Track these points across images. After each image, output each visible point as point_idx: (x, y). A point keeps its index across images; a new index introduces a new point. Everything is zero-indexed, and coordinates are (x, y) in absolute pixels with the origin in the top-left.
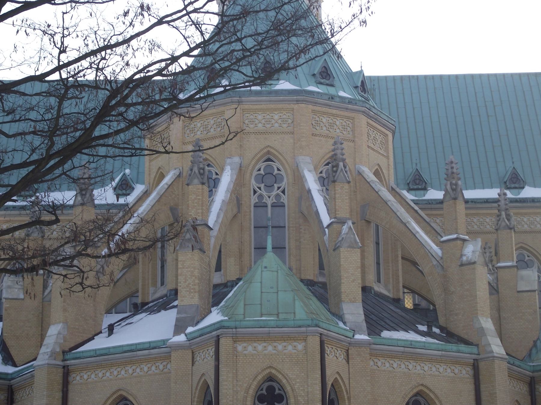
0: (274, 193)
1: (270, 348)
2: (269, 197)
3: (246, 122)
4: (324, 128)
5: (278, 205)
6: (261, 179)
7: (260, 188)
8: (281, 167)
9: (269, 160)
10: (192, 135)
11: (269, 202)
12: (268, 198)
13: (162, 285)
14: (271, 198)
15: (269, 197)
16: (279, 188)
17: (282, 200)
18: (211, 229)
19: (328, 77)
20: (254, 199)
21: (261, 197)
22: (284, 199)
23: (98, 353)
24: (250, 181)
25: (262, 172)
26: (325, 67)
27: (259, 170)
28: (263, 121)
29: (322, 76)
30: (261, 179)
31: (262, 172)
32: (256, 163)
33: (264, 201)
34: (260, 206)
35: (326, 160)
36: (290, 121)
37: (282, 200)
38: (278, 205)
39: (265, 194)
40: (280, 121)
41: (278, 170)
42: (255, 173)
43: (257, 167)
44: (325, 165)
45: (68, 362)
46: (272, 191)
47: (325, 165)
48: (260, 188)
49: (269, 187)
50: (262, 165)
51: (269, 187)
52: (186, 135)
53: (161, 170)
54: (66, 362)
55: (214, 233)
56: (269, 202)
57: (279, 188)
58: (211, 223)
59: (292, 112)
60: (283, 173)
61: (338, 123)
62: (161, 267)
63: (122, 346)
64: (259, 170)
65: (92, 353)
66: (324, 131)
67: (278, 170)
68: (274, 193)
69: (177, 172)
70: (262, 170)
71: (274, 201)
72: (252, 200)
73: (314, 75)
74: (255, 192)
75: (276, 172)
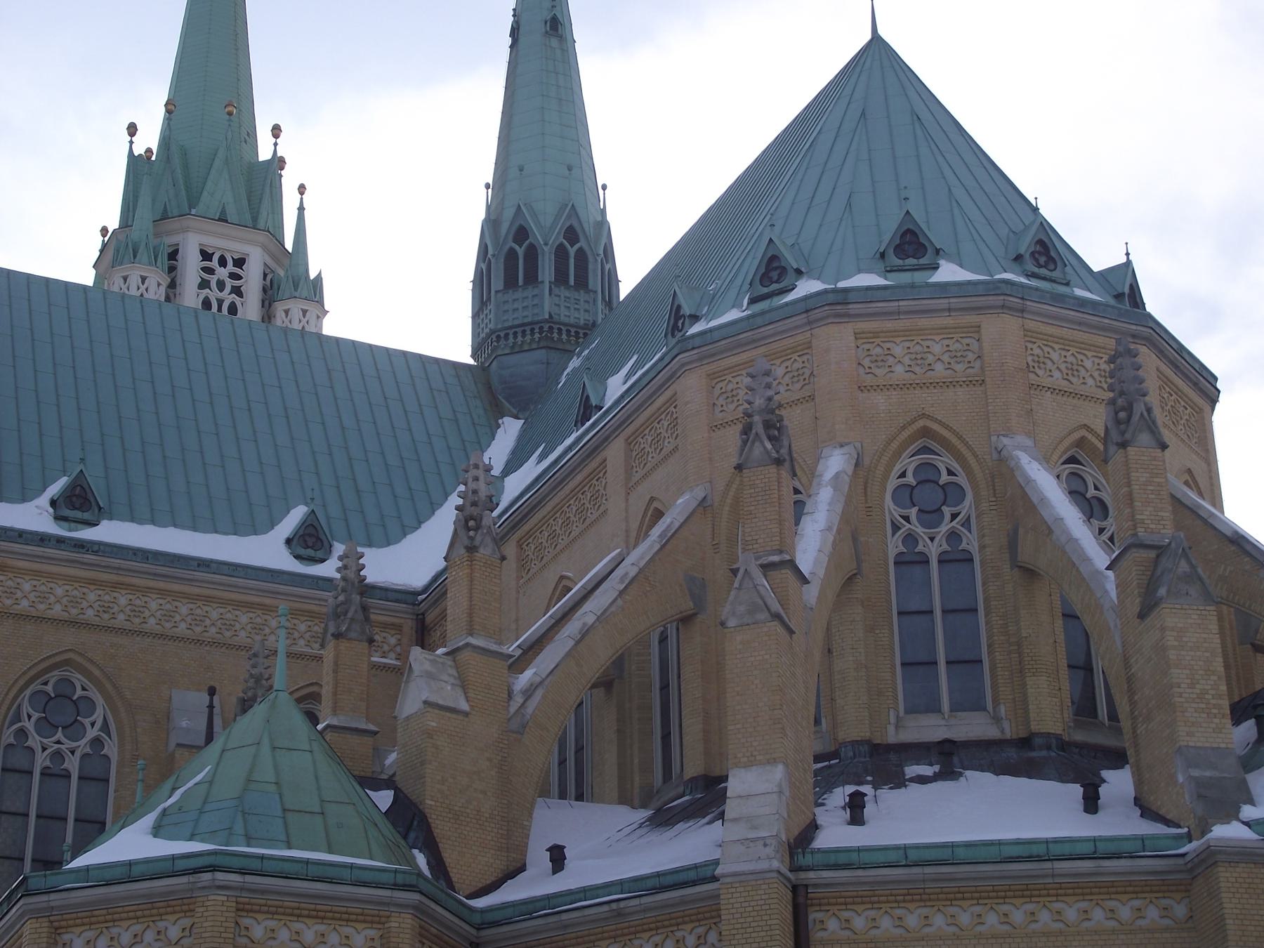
0: (944, 528)
1: (1153, 913)
2: (932, 539)
3: (866, 362)
4: (1057, 374)
5: (956, 559)
6: (906, 494)
7: (907, 519)
8: (956, 466)
9: (925, 450)
10: (732, 407)
11: (934, 551)
12: (929, 541)
13: (664, 782)
14: (936, 540)
15: (932, 539)
16: (954, 516)
17: (964, 545)
18: (805, 580)
19: (1052, 267)
20: (894, 546)
21: (911, 539)
22: (971, 542)
23: (913, 855)
24: (882, 499)
25: (910, 479)
26: (1041, 242)
27: (903, 475)
28: (907, 361)
29: (1037, 260)
30: (906, 494)
31: (910, 479)
32: (897, 455)
33: (920, 548)
34: (911, 561)
35: (1064, 452)
36: (971, 356)
37: (964, 545)
38: (956, 559)
39: (920, 530)
40: (946, 358)
41: (950, 473)
42: (893, 483)
43: (897, 469)
44: (1064, 463)
45: (811, 875)
46: (937, 524)
47: (1064, 463)
48: (907, 519)
49: (931, 516)
50: (909, 463)
51: (931, 516)
52: (718, 409)
53: (655, 504)
54: (802, 875)
55: (811, 593)
56: (934, 551)
57: (954, 516)
58: (805, 565)
59: (976, 335)
60: (962, 479)
61: (1088, 364)
62: (663, 738)
63: (1000, 843)
64: (903, 475)
65: (892, 856)
66: (1057, 379)
67: (950, 473)
68: (944, 528)
69: (700, 493)
70: (910, 474)
71: (945, 547)
72: (890, 546)
73: (1018, 258)
74: (896, 528)
75: (944, 478)
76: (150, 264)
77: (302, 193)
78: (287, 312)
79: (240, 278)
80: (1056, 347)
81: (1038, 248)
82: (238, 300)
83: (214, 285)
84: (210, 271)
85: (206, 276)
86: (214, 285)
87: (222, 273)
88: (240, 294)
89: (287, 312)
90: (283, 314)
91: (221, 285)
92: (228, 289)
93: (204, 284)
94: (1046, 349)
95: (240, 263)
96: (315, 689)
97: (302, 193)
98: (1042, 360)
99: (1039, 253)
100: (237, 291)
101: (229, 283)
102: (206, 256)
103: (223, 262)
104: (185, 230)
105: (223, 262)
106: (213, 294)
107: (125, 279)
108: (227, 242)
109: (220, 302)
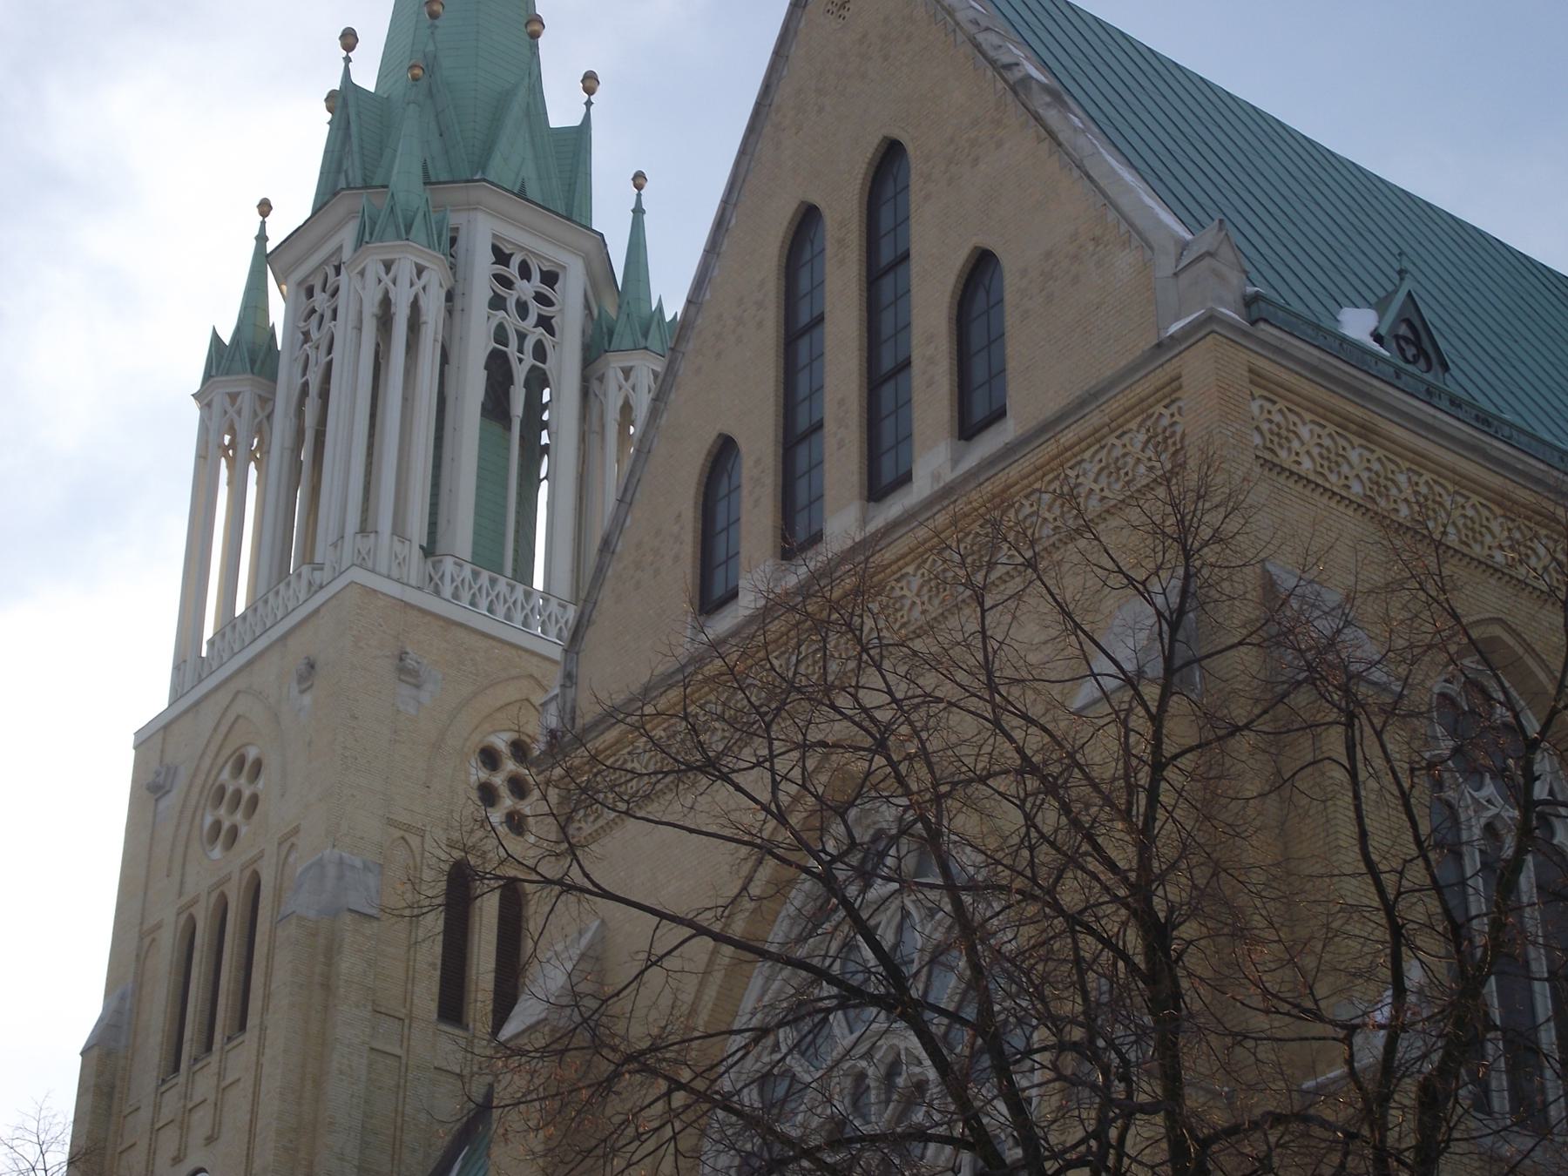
29: (1402, 350)
76: (399, 237)
77: (639, 187)
78: (627, 372)
79: (549, 303)
80: (1308, 416)
81: (1403, 330)
82: (548, 340)
83: (511, 304)
84: (506, 282)
85: (501, 290)
86: (511, 304)
87: (526, 289)
88: (551, 332)
89: (627, 372)
90: (621, 375)
91: (522, 309)
92: (533, 318)
93: (497, 303)
94: (1341, 442)
95: (550, 278)
96: (305, 686)
97: (639, 187)
98: (1284, 432)
99: (1405, 339)
100: (545, 322)
101: (535, 309)
102: (501, 257)
103: (525, 272)
104: (472, 207)
105: (525, 272)
106: (512, 321)
107: (388, 266)
108: (538, 241)
109: (522, 337)
